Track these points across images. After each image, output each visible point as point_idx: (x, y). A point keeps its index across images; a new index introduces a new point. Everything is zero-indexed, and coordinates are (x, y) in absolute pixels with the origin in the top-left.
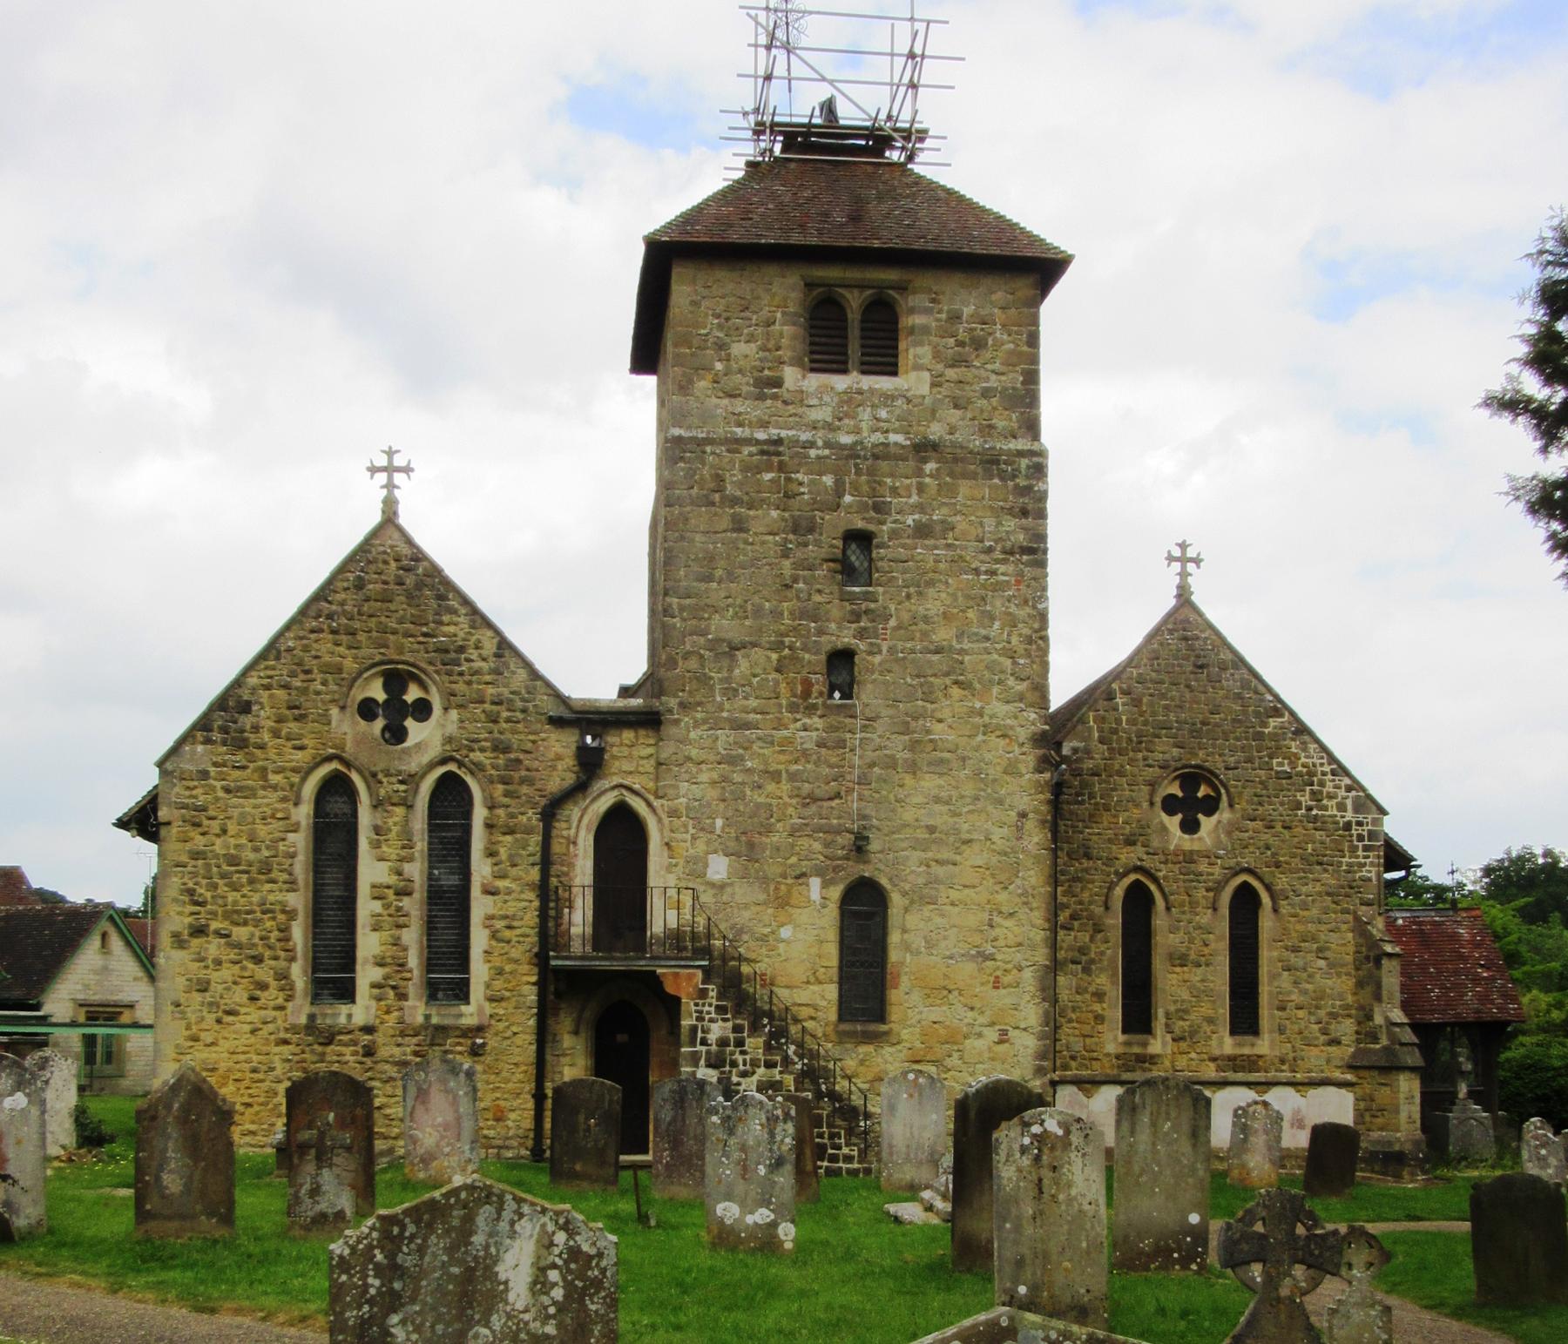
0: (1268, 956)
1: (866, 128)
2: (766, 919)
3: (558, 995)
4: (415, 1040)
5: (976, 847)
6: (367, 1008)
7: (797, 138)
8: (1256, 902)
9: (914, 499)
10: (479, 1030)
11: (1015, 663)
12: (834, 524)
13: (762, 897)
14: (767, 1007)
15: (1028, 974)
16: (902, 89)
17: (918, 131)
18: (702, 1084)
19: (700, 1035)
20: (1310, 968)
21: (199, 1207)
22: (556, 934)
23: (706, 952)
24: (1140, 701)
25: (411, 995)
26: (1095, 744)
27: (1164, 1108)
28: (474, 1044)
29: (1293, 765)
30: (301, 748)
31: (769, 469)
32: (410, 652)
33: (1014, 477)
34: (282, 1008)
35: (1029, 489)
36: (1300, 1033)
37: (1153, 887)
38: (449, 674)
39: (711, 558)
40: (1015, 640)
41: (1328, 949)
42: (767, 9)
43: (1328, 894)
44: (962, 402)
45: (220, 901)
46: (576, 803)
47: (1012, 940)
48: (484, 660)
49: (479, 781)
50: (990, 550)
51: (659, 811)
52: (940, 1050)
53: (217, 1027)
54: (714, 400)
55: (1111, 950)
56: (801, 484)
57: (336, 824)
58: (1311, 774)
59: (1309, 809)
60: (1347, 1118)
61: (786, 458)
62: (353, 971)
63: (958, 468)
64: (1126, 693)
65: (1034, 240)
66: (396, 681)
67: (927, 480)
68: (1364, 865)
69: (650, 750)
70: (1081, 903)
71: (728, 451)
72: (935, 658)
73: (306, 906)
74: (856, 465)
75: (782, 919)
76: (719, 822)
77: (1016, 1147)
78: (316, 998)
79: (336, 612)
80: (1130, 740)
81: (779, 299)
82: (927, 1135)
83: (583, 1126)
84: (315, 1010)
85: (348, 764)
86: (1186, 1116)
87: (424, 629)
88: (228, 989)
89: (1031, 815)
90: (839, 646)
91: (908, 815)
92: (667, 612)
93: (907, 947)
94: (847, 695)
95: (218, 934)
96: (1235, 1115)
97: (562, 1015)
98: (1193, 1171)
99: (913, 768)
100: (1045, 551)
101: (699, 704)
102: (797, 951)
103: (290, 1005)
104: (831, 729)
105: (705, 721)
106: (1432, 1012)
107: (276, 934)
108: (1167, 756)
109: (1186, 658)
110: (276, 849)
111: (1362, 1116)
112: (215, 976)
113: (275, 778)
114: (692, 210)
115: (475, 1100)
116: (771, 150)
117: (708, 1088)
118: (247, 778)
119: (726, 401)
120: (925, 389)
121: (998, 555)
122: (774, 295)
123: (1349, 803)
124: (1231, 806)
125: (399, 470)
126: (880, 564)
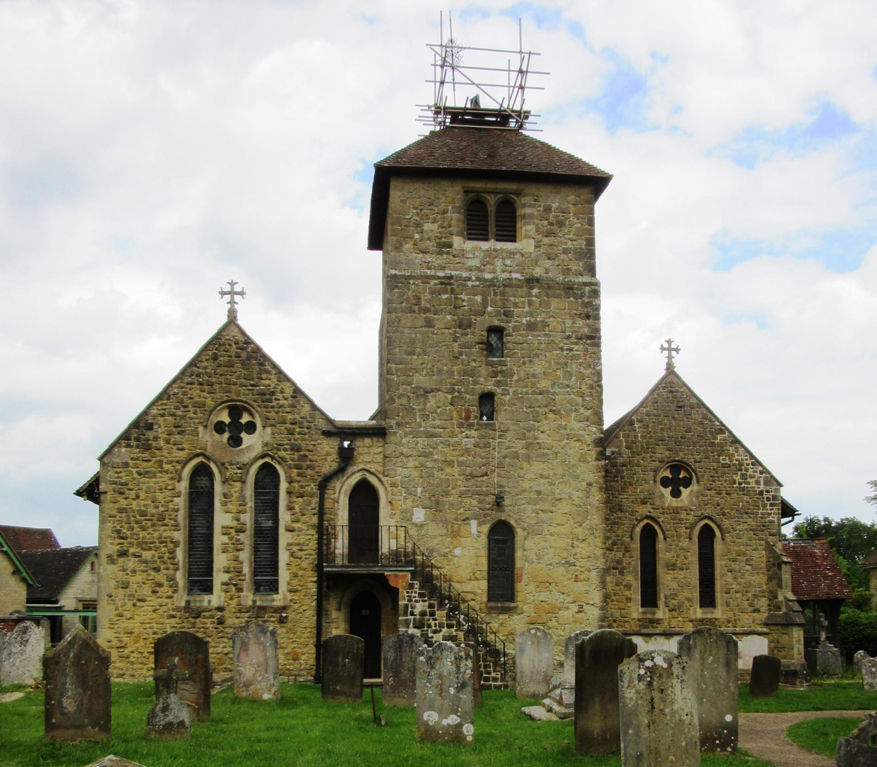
0: (720, 564)
1: (496, 110)
2: (446, 544)
3: (329, 588)
4: (247, 615)
5: (564, 502)
6: (220, 597)
7: (456, 115)
8: (712, 535)
9: (527, 309)
10: (284, 608)
11: (584, 400)
12: (482, 323)
13: (444, 532)
14: (447, 594)
15: (594, 574)
16: (516, 89)
17: (525, 112)
18: (412, 637)
19: (410, 609)
20: (742, 573)
21: (87, 720)
22: (327, 553)
23: (413, 562)
24: (648, 426)
25: (245, 589)
26: (624, 449)
27: (708, 648)
28: (281, 616)
30: (182, 449)
31: (446, 293)
32: (244, 395)
33: (582, 297)
34: (170, 597)
35: (590, 303)
36: (738, 606)
37: (656, 527)
38: (266, 407)
39: (413, 342)
40: (584, 387)
41: (752, 560)
42: (441, 46)
43: (752, 530)
44: (553, 256)
45: (135, 537)
46: (338, 479)
47: (585, 554)
48: (286, 399)
49: (283, 467)
50: (569, 337)
51: (386, 484)
52: (545, 617)
53: (133, 609)
54: (415, 255)
55: (635, 561)
56: (463, 301)
57: (202, 493)
58: (741, 465)
59: (740, 484)
60: (765, 652)
61: (455, 287)
62: (212, 576)
63: (551, 292)
64: (640, 421)
65: (591, 168)
66: (235, 411)
67: (534, 298)
68: (770, 514)
69: (380, 449)
70: (617, 536)
71: (423, 283)
72: (540, 397)
73: (184, 539)
74: (494, 290)
75: (455, 544)
76: (419, 490)
77: (635, 676)
78: (190, 591)
79: (201, 373)
80: (643, 447)
81: (450, 198)
82: (542, 665)
83: (341, 664)
84: (190, 598)
85: (208, 458)
86: (722, 654)
87: (252, 382)
88: (140, 587)
89: (594, 485)
91: (526, 485)
92: (389, 372)
93: (526, 559)
94: (490, 418)
95: (134, 555)
97: (331, 600)
98: (728, 687)
99: (528, 459)
100: (599, 338)
101: (407, 423)
102: (465, 563)
103: (175, 595)
104: (482, 437)
105: (411, 433)
106: (804, 594)
107: (167, 554)
108: (663, 456)
109: (672, 402)
110: (168, 507)
111: (773, 651)
112: (132, 579)
113: (166, 467)
114: (402, 150)
115: (276, 649)
116: (444, 122)
117: (416, 640)
118: (151, 466)
119: (421, 255)
120: (531, 249)
121: (573, 340)
122: (447, 197)
123: (762, 480)
124: (698, 482)
125: (237, 293)
126: (508, 345)
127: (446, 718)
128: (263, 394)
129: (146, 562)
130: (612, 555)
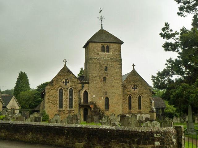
0: (142, 102)
10: (74, 110)
55: (128, 102)
94: (105, 81)
95: (51, 102)
130: (123, 101)
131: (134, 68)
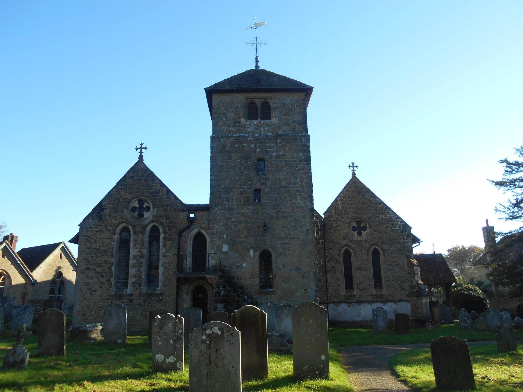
4: (143, 298)
9: (275, 149)
10: (161, 294)
29: (385, 217)
30: (116, 220)
34: (108, 290)
37: (351, 250)
43: (398, 250)
50: (296, 161)
58: (391, 219)
59: (391, 228)
66: (141, 202)
69: (207, 217)
70: (332, 255)
76: (225, 236)
90: (257, 188)
95: (92, 269)
96: (373, 311)
102: (247, 268)
120: (277, 122)
125: (144, 148)
127: (168, 358)
128: (154, 193)
129: (98, 273)
131: (141, 158)
